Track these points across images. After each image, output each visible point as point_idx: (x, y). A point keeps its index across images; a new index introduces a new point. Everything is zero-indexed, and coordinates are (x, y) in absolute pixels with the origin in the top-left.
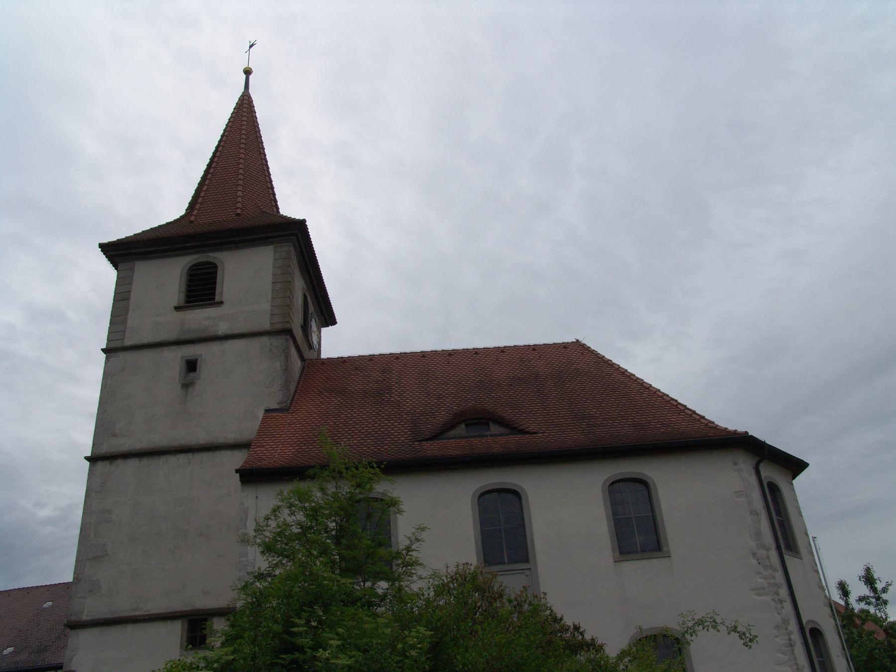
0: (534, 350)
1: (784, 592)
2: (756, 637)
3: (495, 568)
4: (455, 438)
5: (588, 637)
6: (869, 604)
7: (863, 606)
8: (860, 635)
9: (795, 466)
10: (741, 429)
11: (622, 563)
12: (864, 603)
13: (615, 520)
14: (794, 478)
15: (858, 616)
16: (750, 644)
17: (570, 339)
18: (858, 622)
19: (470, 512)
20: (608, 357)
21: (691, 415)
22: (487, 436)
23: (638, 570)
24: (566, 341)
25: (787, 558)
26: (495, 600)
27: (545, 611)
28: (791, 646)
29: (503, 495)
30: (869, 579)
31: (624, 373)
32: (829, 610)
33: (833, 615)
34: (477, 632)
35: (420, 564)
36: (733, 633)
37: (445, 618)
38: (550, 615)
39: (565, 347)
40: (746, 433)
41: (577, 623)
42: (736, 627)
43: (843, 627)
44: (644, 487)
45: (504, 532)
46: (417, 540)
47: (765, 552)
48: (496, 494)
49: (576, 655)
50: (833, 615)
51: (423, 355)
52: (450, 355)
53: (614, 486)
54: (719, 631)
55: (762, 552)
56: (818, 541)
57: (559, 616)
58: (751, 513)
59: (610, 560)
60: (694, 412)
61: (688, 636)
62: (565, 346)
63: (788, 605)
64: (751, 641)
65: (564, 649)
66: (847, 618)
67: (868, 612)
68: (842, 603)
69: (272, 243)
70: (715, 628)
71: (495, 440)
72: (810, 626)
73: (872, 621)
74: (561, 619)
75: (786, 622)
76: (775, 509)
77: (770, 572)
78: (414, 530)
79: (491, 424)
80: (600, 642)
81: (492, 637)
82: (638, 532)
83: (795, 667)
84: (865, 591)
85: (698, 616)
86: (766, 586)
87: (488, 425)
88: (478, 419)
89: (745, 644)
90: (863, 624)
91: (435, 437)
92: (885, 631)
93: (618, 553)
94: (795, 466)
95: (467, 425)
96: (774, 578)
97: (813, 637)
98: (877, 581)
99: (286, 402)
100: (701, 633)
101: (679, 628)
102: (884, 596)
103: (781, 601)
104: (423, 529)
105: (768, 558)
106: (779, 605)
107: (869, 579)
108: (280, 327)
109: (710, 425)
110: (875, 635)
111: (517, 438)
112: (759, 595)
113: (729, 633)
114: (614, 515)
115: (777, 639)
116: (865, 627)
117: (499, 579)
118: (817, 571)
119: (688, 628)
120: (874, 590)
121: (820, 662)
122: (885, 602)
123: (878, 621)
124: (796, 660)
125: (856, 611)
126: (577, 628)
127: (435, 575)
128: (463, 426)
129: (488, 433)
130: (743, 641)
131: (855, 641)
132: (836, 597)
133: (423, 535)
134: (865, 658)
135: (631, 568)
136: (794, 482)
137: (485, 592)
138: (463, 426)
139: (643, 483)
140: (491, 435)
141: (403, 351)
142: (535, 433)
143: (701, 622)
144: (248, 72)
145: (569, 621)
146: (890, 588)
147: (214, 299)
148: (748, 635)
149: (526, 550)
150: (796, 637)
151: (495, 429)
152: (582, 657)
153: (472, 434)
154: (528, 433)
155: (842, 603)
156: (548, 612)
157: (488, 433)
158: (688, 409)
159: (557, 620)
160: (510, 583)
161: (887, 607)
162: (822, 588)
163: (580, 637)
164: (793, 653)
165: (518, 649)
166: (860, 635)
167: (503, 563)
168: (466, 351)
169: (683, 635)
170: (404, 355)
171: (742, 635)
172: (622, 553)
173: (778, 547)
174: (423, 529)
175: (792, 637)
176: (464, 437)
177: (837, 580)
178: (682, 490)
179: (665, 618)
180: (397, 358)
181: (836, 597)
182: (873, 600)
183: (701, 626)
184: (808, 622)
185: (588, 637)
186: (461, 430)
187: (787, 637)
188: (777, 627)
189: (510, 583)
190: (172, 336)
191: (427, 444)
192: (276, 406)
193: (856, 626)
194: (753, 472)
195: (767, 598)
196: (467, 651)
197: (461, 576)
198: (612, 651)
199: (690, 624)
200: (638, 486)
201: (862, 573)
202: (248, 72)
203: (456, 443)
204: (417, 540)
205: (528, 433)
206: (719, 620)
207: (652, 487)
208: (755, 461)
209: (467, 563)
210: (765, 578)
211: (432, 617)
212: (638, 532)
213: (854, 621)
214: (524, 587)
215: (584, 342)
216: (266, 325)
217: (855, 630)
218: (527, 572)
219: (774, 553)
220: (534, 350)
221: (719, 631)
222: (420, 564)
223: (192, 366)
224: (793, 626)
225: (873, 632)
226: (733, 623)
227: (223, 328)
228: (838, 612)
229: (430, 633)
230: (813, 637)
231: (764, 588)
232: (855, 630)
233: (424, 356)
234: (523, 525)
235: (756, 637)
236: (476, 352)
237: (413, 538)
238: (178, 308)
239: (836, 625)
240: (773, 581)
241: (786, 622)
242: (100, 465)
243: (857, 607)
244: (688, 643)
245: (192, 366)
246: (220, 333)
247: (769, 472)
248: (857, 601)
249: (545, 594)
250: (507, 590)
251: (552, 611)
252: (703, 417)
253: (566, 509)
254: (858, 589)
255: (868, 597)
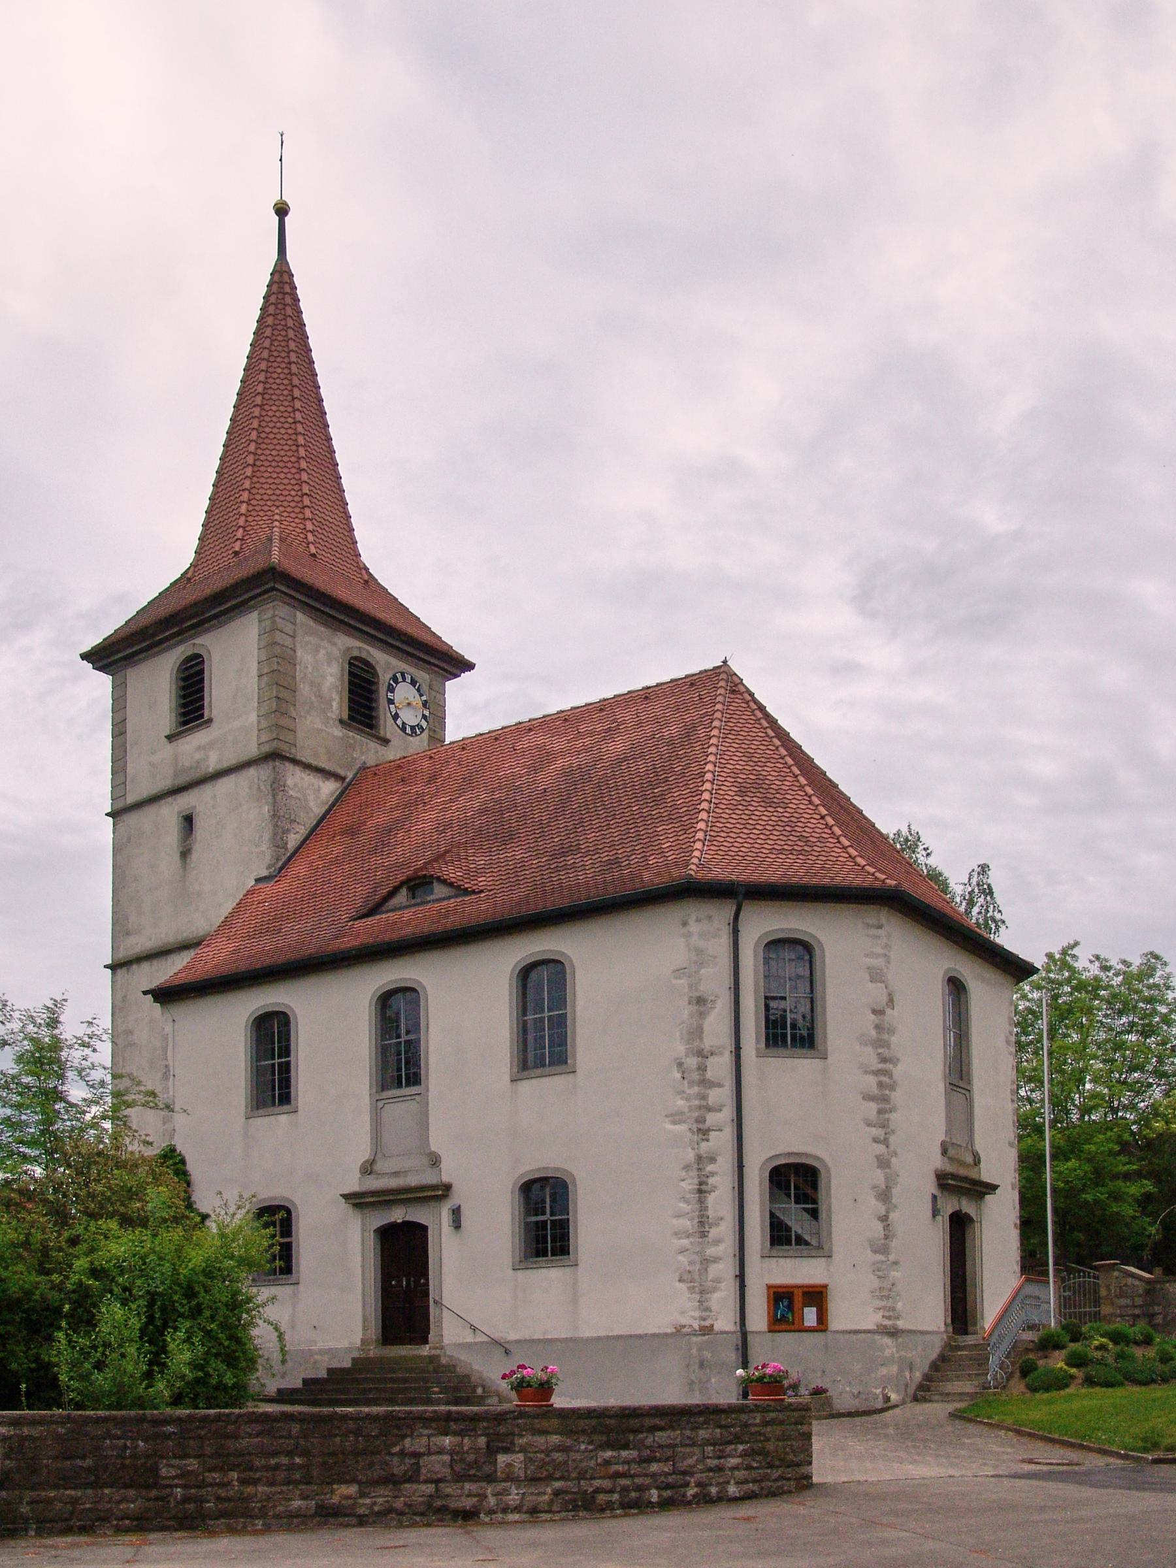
23: (544, 1088)
69: (254, 608)
86: (686, 1110)
91: (371, 912)
99: (273, 865)
108: (267, 748)
112: (674, 1123)
115: (683, 1184)
135: (531, 1088)
144: (282, 211)
147: (202, 716)
176: (407, 907)
188: (686, 1167)
190: (165, 783)
192: (265, 873)
202: (282, 211)
207: (817, 952)
210: (687, 1100)
216: (253, 751)
223: (188, 821)
227: (213, 763)
231: (683, 1113)
238: (170, 738)
242: (121, 972)
245: (188, 821)
246: (211, 770)
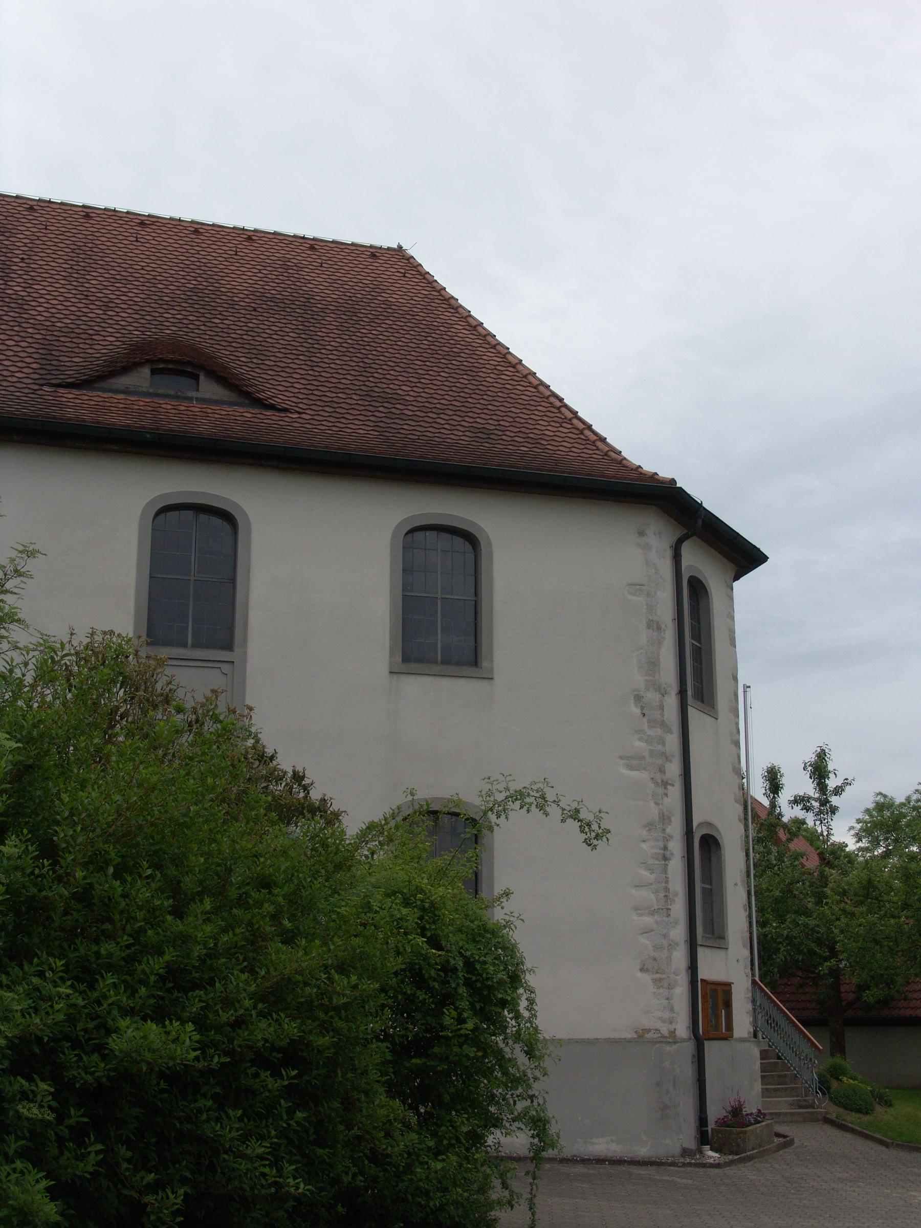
0: (312, 248)
1: (674, 769)
2: (608, 831)
3: (164, 652)
4: (127, 391)
5: (315, 795)
6: (807, 809)
7: (797, 812)
8: (780, 859)
9: (744, 557)
10: (665, 473)
11: (403, 678)
12: (800, 807)
13: (404, 597)
14: (737, 577)
15: (785, 826)
16: (595, 842)
17: (388, 241)
18: (782, 835)
19: (135, 540)
20: (451, 290)
21: (583, 431)
22: (190, 399)
23: (434, 697)
24: (377, 243)
25: (691, 711)
26: (155, 707)
27: (245, 740)
28: (665, 858)
29: (203, 517)
30: (819, 770)
31: (475, 327)
32: (740, 809)
33: (746, 819)
34: (108, 757)
35: (18, 621)
36: (570, 821)
37: (49, 723)
38: (254, 747)
39: (373, 255)
40: (673, 481)
41: (299, 769)
42: (577, 811)
43: (758, 841)
44: (469, 547)
45: (194, 581)
46: (17, 573)
47: (657, 697)
48: (190, 513)
49: (288, 824)
50: (746, 819)
51: (87, 213)
52: (142, 224)
53: (416, 533)
54: (547, 814)
55: (652, 697)
56: (751, 693)
57: (269, 751)
58: (649, 626)
59: (383, 667)
60: (589, 427)
61: (492, 817)
62: (374, 253)
63: (675, 792)
64: (597, 837)
65: (269, 809)
66: (767, 828)
67: (803, 822)
68: (766, 802)
70: (541, 808)
71: (205, 408)
72: (704, 831)
73: (806, 838)
74: (272, 758)
75: (665, 818)
76: (692, 627)
77: (658, 731)
78: (14, 554)
79: (202, 378)
80: (335, 807)
81: (136, 769)
82: (442, 627)
83: (661, 895)
84: (808, 788)
85: (514, 787)
86: (646, 754)
87: (196, 378)
88: (180, 363)
89: (587, 842)
90: (789, 840)
92: (821, 855)
93: (398, 658)
94: (744, 557)
95: (154, 372)
96: (664, 744)
97: (705, 848)
98: (831, 775)
100: (516, 813)
101: (477, 801)
102: (834, 800)
103: (665, 784)
104: (30, 554)
105: (661, 707)
106: (661, 790)
107: (819, 770)
109: (620, 462)
110: (804, 861)
111: (248, 413)
112: (631, 768)
113: (563, 821)
114: (404, 589)
116: (792, 846)
117: (169, 671)
118: (737, 744)
119: (495, 802)
120: (822, 787)
121: (704, 889)
122: (834, 810)
123: (813, 838)
124: (667, 882)
125: (785, 819)
126: (298, 777)
127: (48, 647)
128: (146, 371)
129: (194, 394)
130: (584, 836)
131: (770, 866)
132: (758, 791)
133: (31, 565)
134: (777, 893)
136: (736, 585)
137: (137, 690)
138: (146, 371)
139: (470, 539)
140: (197, 399)
141: (46, 197)
142: (285, 410)
143: (519, 796)
145: (285, 763)
146: (848, 788)
148: (595, 827)
149: (231, 628)
150: (677, 847)
151: (209, 388)
152: (297, 831)
153: (160, 391)
154: (272, 407)
155: (766, 802)
156: (250, 742)
157: (194, 394)
158: (580, 419)
159: (265, 758)
160: (190, 681)
161: (835, 817)
162: (737, 771)
163: (302, 795)
164: (665, 871)
165: (181, 796)
166: (780, 859)
167: (184, 645)
168: (176, 224)
169: (485, 813)
170: (46, 205)
171: (585, 826)
172: (406, 659)
173: (682, 693)
174: (30, 554)
175: (671, 845)
177: (766, 764)
178: (546, 571)
179: (461, 786)
180: (31, 208)
181: (758, 791)
182: (816, 804)
183: (518, 803)
184: (701, 825)
185: (315, 795)
186: (141, 378)
187: (661, 844)
188: (650, 826)
189: (190, 681)
191: (68, 395)
193: (778, 842)
194: (669, 554)
195: (643, 776)
196: (83, 787)
197: (96, 654)
198: (352, 826)
199: (500, 797)
200: (459, 542)
201: (811, 757)
203: (131, 401)
204: (17, 573)
205: (272, 407)
206: (550, 797)
207: (483, 544)
208: (678, 534)
209: (112, 632)
210: (647, 741)
211: (24, 716)
212: (442, 627)
213: (776, 833)
214: (213, 691)
215: (411, 252)
217: (774, 849)
218: (226, 668)
219: (672, 702)
220: (312, 248)
221: (547, 814)
222: (18, 621)
224: (676, 828)
225: (802, 855)
226: (575, 805)
228: (755, 816)
229: (16, 745)
230: (705, 848)
231: (643, 758)
232: (774, 849)
233: (87, 216)
234: (233, 581)
235: (608, 831)
236: (197, 229)
237: (10, 569)
239: (747, 837)
240: (660, 747)
241: (665, 818)
243: (789, 813)
244: (491, 829)
247: (698, 560)
248: (790, 802)
249: (251, 709)
250: (180, 693)
251: (257, 741)
252: (603, 440)
253: (318, 561)
254: (797, 783)
255: (809, 798)
